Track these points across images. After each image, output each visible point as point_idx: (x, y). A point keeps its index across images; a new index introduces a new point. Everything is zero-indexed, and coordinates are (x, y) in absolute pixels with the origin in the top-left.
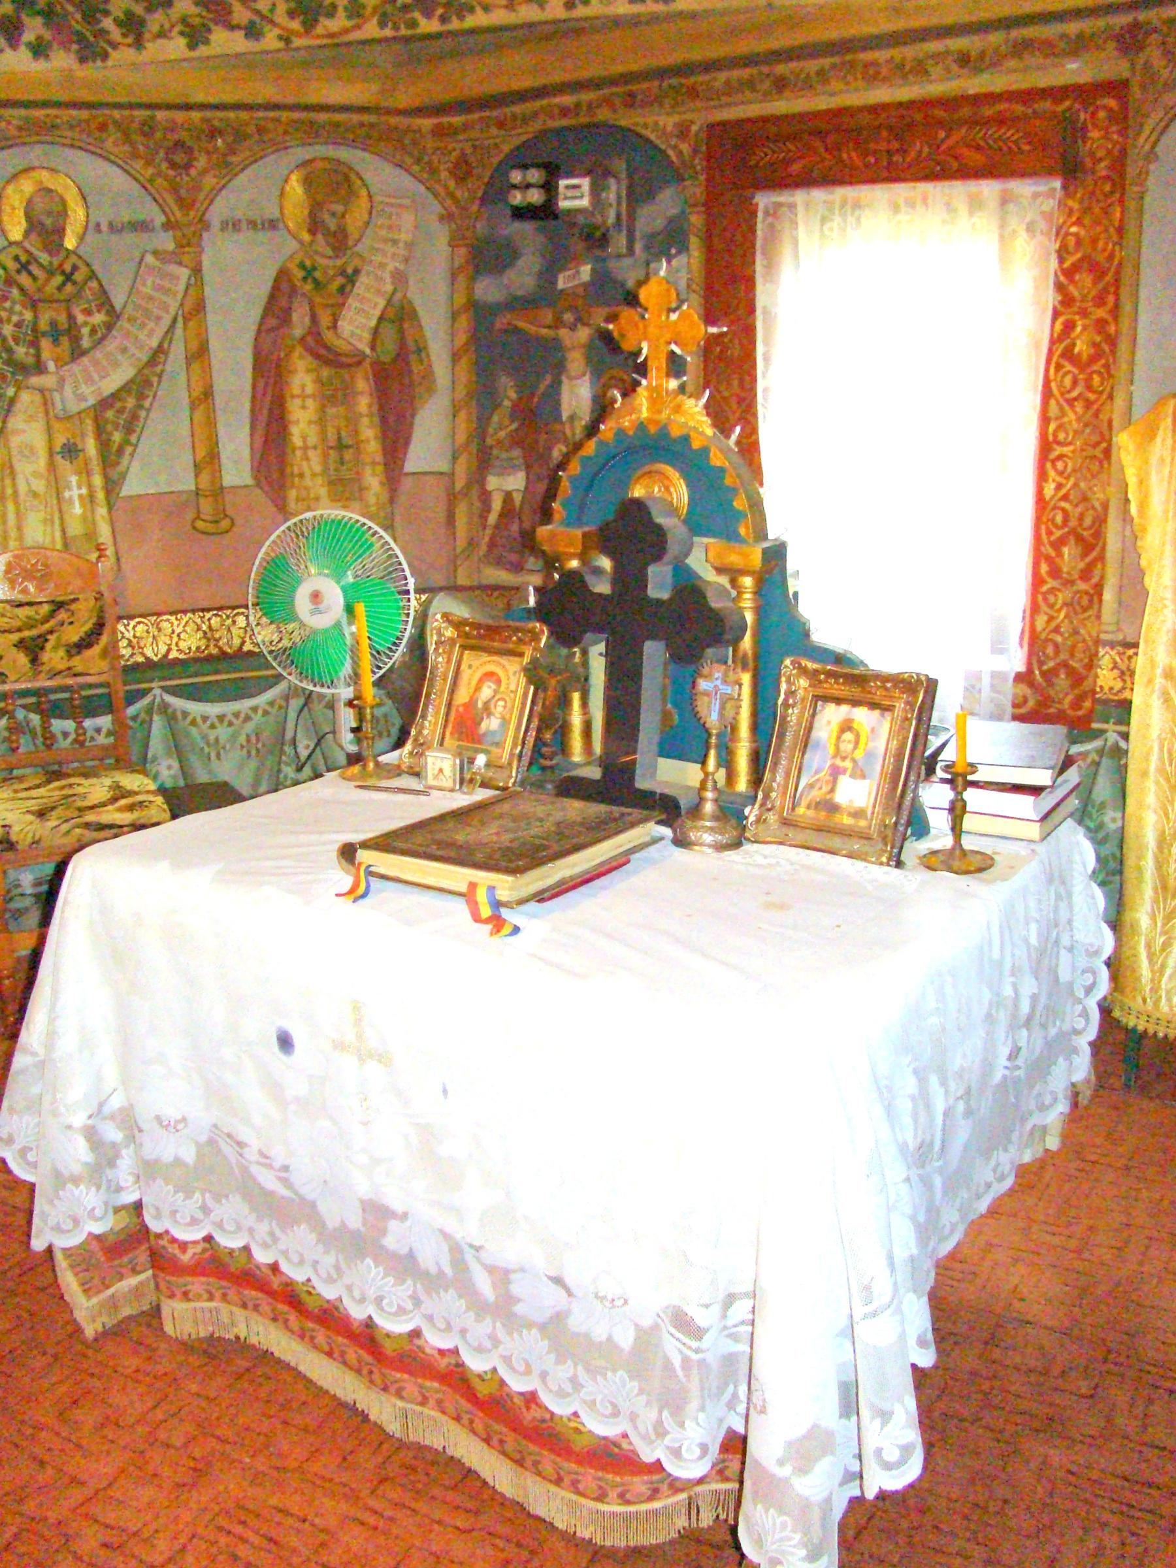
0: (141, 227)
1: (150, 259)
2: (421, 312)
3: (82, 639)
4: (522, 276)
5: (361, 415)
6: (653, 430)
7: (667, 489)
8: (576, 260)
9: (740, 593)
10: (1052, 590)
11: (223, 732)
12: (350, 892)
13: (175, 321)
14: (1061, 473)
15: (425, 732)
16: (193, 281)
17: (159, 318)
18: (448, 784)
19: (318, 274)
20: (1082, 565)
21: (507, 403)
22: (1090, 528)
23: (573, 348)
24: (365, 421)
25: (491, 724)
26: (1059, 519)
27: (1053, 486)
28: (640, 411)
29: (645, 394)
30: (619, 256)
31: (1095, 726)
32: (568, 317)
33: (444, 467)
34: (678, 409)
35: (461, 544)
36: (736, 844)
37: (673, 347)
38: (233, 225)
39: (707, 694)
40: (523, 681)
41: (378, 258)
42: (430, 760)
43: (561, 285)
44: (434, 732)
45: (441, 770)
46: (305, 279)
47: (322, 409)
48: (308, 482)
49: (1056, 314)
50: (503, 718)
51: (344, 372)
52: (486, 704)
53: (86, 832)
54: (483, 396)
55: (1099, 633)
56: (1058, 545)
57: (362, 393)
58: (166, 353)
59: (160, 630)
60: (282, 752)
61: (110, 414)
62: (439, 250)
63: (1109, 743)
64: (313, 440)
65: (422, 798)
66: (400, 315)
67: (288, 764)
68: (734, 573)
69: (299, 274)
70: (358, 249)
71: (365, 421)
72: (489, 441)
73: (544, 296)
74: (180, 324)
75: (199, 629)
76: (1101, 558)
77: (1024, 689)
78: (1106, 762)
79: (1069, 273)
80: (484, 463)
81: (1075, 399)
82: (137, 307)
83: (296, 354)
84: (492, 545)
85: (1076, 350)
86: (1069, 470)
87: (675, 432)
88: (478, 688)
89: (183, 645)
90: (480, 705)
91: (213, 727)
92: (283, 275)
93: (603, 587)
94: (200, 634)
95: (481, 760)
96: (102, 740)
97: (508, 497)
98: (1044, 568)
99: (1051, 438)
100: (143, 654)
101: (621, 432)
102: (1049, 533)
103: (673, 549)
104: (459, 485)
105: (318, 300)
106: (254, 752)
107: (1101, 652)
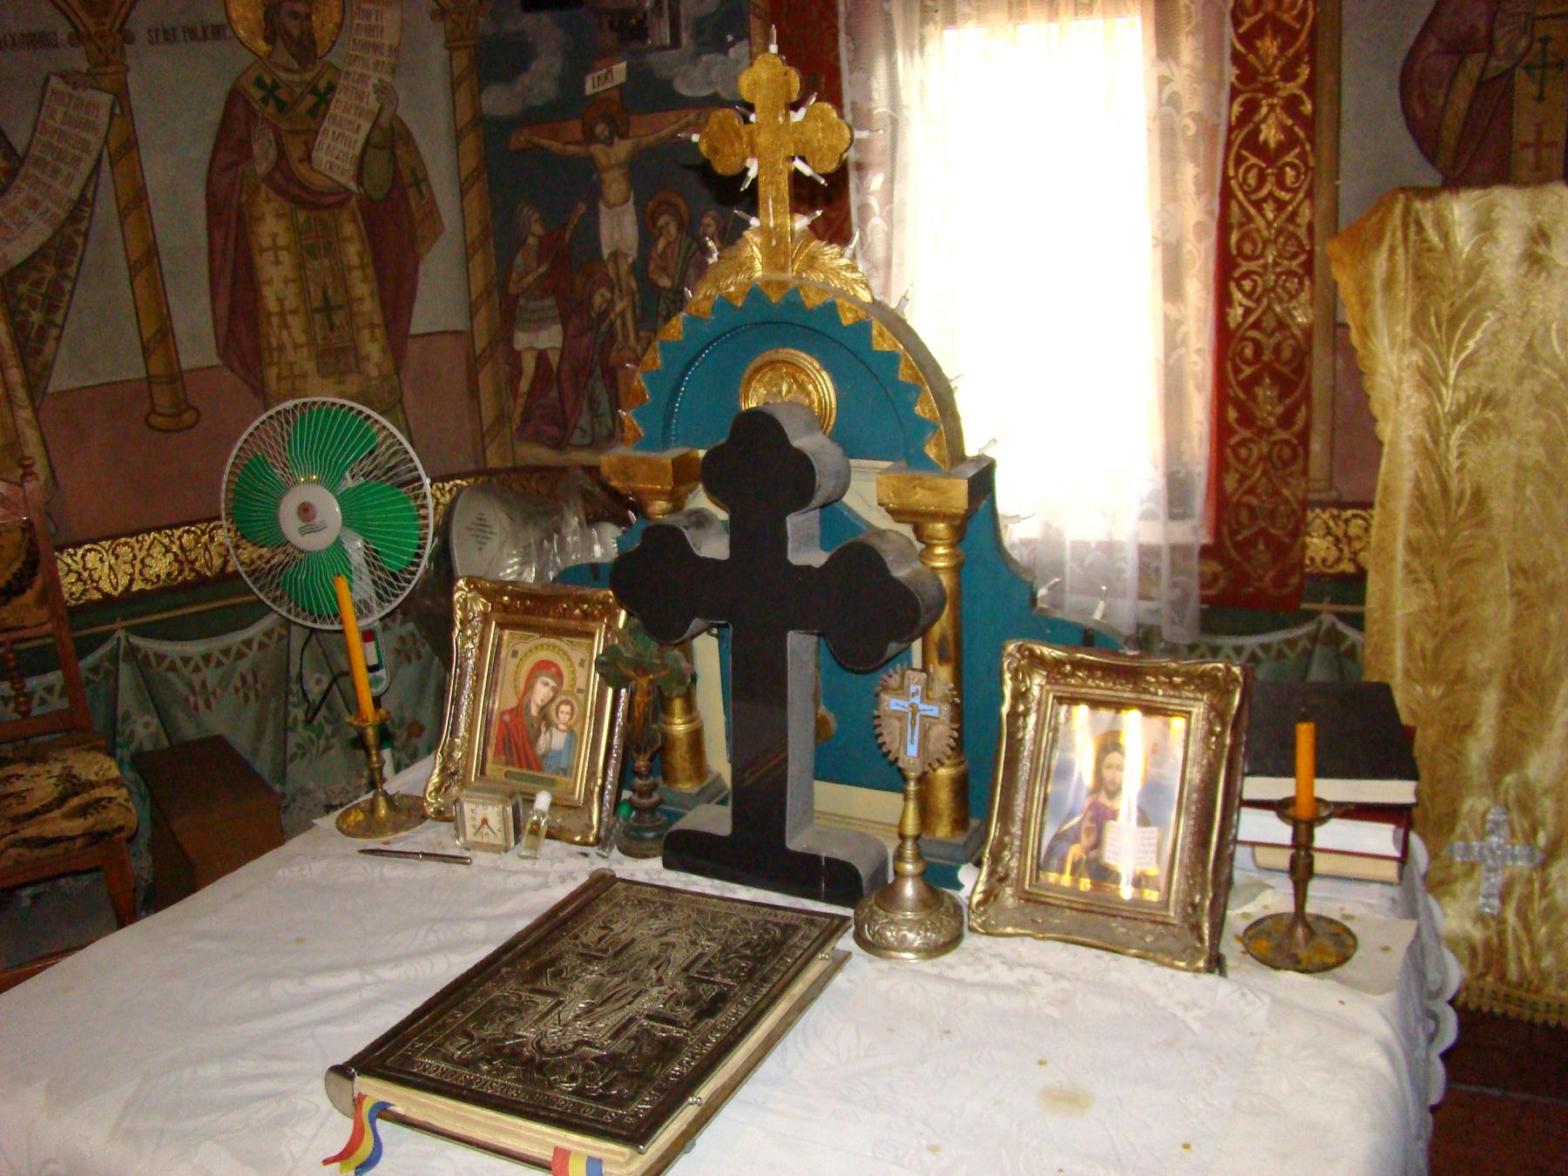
0: (39, 40)
1: (55, 83)
2: (415, 130)
3: (9, 583)
4: (541, 79)
5: (351, 269)
6: (775, 297)
7: (802, 387)
8: (609, 56)
9: (929, 546)
10: (1243, 443)
11: (211, 676)
12: (342, 1157)
13: (99, 162)
14: (1248, 295)
15: (458, 755)
16: (118, 111)
17: (77, 161)
18: (499, 840)
19: (282, 94)
20: (1280, 410)
21: (531, 241)
22: (1290, 361)
23: (610, 167)
24: (357, 274)
25: (551, 740)
26: (1249, 352)
27: (1240, 311)
28: (751, 268)
29: (758, 240)
30: (663, 48)
31: (1305, 606)
32: (601, 129)
33: (460, 325)
34: (812, 262)
35: (488, 414)
36: (954, 941)
37: (798, 164)
38: (164, 36)
39: (900, 717)
40: (595, 678)
41: (357, 69)
42: (467, 807)
43: (589, 89)
44: (468, 754)
45: (485, 821)
46: (265, 101)
47: (300, 266)
48: (291, 356)
49: (1234, 93)
50: (570, 731)
51: (325, 215)
52: (543, 709)
53: (24, 851)
54: (499, 235)
55: (1307, 491)
56: (1249, 385)
57: (350, 239)
58: (92, 205)
59: (117, 557)
60: (288, 692)
61: (23, 288)
62: (435, 58)
63: (1324, 627)
64: (291, 303)
65: (460, 868)
66: (390, 139)
67: (295, 705)
68: (917, 519)
69: (257, 93)
70: (331, 58)
71: (357, 274)
72: (513, 290)
73: (567, 101)
74: (106, 166)
75: (168, 550)
76: (1307, 397)
77: (1214, 566)
78: (1319, 649)
79: (1248, 39)
80: (509, 315)
81: (1264, 200)
82: (48, 147)
83: (262, 196)
84: (526, 418)
85: (1262, 137)
86: (1259, 290)
87: (813, 300)
88: (529, 687)
89: (149, 573)
90: (534, 711)
91: (197, 669)
92: (235, 96)
93: (715, 547)
94: (170, 557)
95: (543, 801)
96: (58, 703)
97: (542, 357)
98: (1232, 414)
99: (1234, 252)
100: (97, 589)
101: (724, 304)
102: (1237, 371)
103: (825, 486)
104: (480, 344)
105: (284, 126)
106: (252, 695)
107: (1310, 515)
